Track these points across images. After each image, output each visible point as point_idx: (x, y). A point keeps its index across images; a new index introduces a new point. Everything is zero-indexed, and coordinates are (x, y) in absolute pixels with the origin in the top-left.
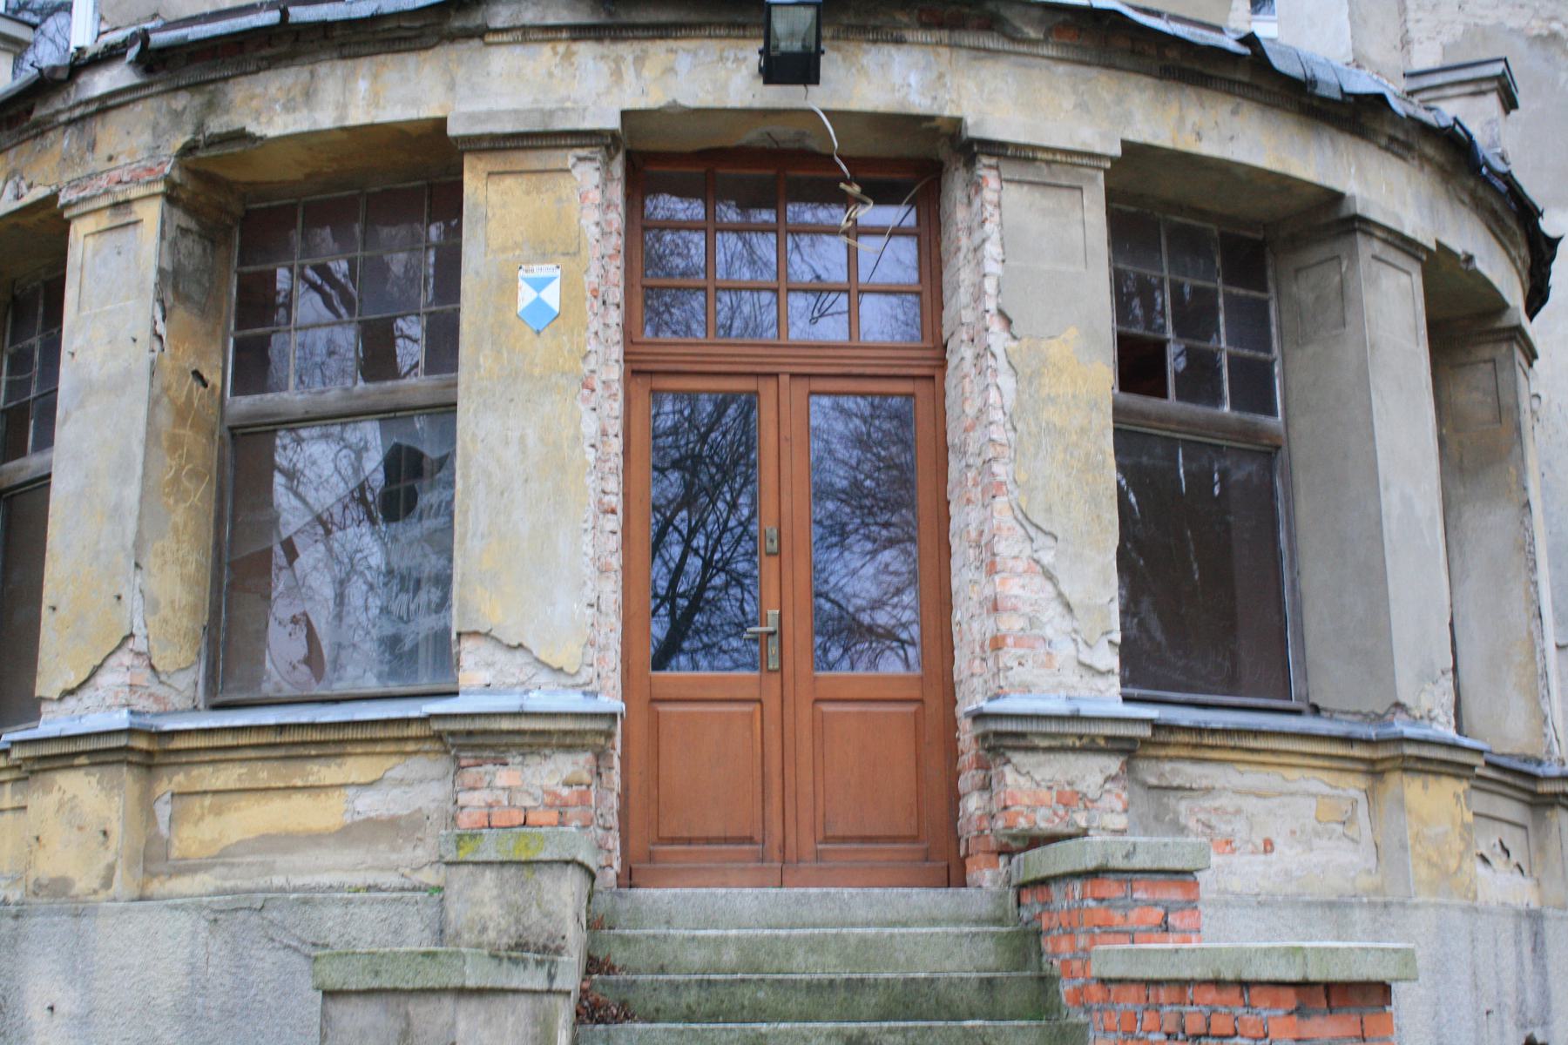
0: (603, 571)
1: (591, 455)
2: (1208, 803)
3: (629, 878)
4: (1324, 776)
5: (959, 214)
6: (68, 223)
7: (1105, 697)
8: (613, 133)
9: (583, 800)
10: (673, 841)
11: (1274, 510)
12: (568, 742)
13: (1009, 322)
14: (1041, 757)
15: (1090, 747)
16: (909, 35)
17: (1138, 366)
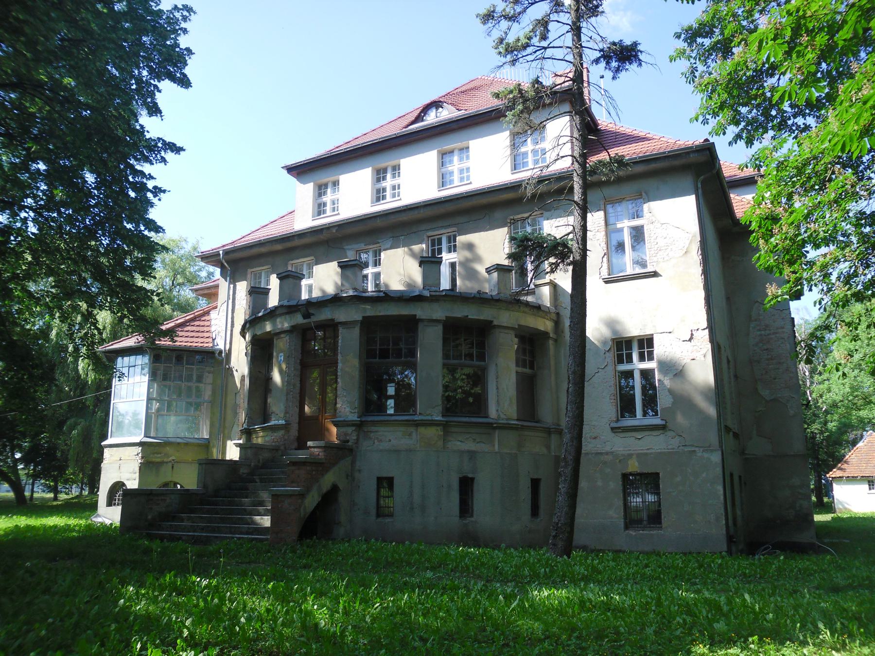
15: (348, 425)
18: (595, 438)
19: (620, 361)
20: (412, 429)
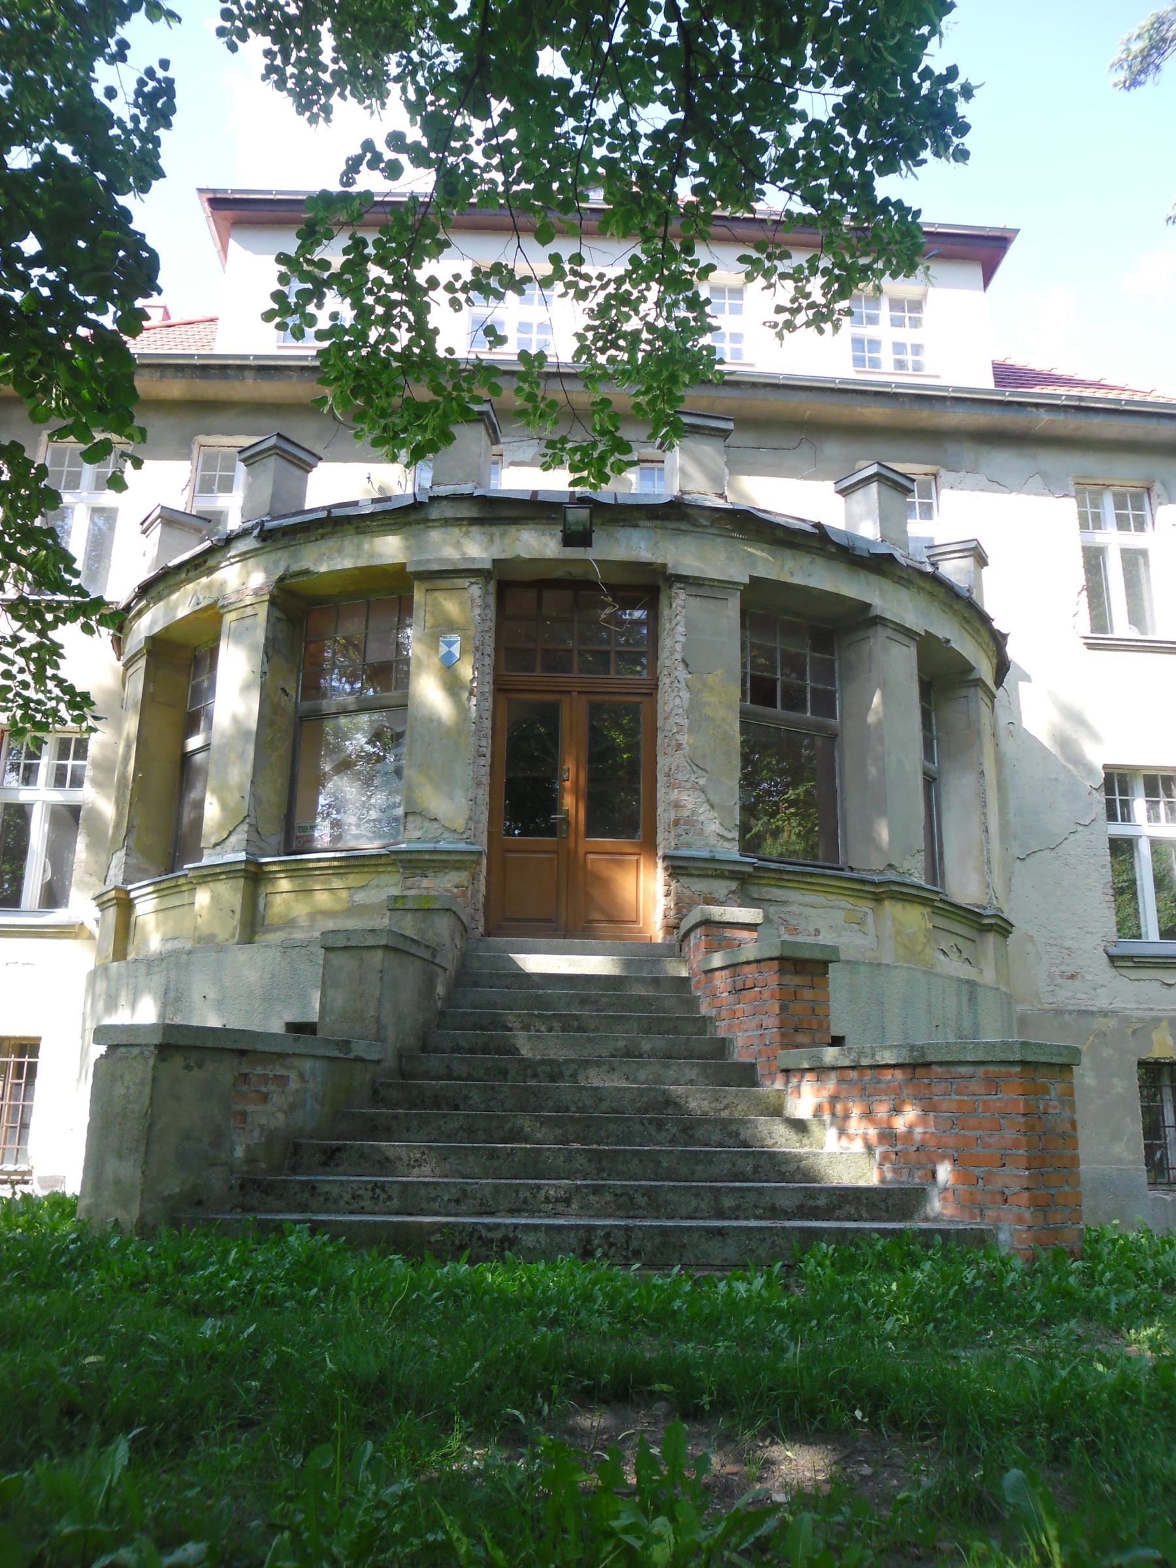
0: (479, 784)
1: (473, 727)
2: (785, 909)
3: (488, 933)
4: (850, 899)
5: (665, 612)
6: (222, 616)
7: (731, 851)
8: (488, 571)
9: (464, 894)
10: (512, 920)
11: (833, 768)
12: (458, 866)
13: (687, 665)
14: (695, 880)
15: (720, 875)
16: (641, 523)
17: (759, 690)
18: (1072, 977)
19: (1112, 816)
20: (865, 906)
